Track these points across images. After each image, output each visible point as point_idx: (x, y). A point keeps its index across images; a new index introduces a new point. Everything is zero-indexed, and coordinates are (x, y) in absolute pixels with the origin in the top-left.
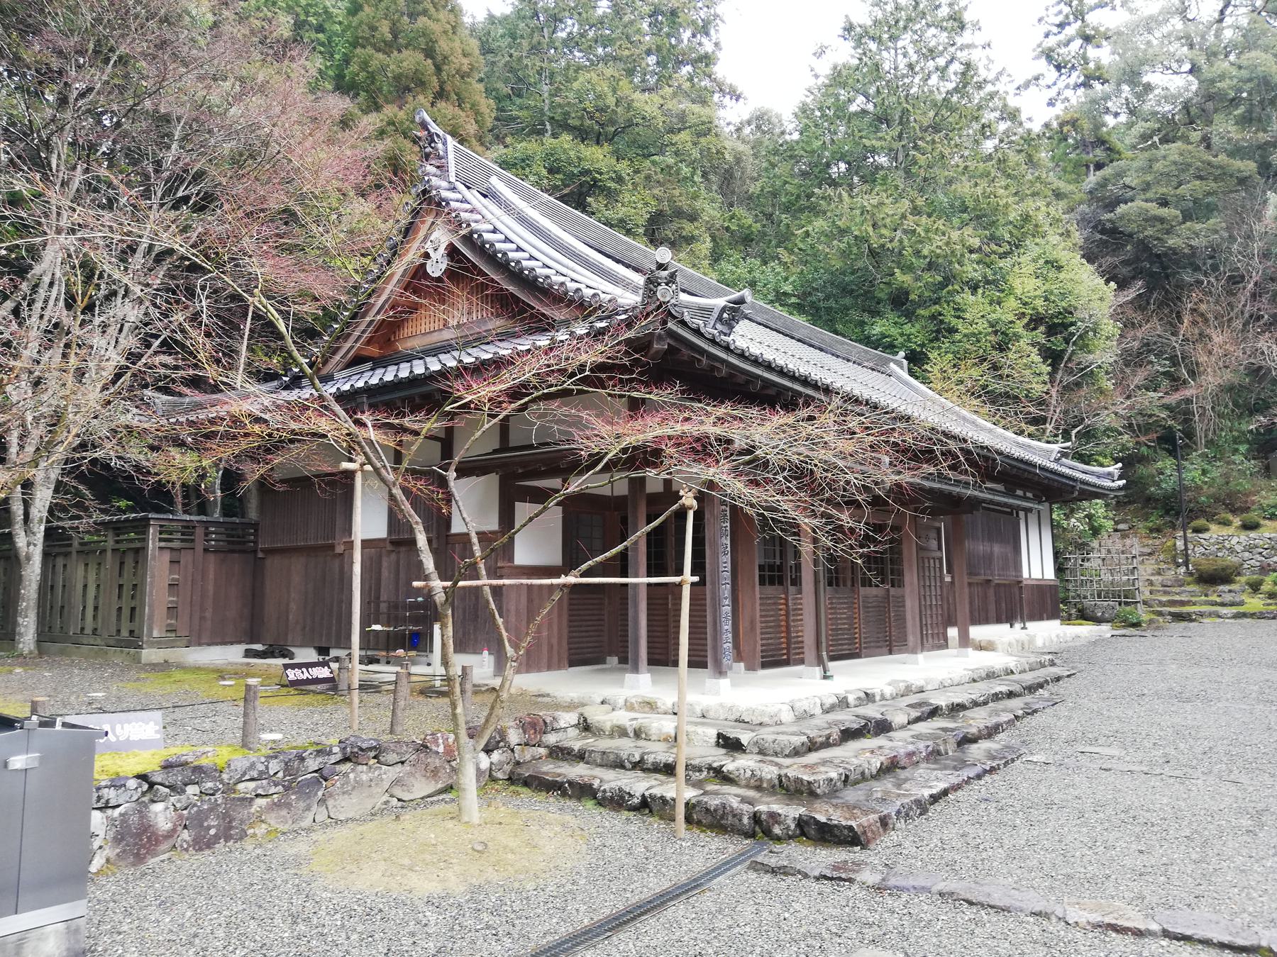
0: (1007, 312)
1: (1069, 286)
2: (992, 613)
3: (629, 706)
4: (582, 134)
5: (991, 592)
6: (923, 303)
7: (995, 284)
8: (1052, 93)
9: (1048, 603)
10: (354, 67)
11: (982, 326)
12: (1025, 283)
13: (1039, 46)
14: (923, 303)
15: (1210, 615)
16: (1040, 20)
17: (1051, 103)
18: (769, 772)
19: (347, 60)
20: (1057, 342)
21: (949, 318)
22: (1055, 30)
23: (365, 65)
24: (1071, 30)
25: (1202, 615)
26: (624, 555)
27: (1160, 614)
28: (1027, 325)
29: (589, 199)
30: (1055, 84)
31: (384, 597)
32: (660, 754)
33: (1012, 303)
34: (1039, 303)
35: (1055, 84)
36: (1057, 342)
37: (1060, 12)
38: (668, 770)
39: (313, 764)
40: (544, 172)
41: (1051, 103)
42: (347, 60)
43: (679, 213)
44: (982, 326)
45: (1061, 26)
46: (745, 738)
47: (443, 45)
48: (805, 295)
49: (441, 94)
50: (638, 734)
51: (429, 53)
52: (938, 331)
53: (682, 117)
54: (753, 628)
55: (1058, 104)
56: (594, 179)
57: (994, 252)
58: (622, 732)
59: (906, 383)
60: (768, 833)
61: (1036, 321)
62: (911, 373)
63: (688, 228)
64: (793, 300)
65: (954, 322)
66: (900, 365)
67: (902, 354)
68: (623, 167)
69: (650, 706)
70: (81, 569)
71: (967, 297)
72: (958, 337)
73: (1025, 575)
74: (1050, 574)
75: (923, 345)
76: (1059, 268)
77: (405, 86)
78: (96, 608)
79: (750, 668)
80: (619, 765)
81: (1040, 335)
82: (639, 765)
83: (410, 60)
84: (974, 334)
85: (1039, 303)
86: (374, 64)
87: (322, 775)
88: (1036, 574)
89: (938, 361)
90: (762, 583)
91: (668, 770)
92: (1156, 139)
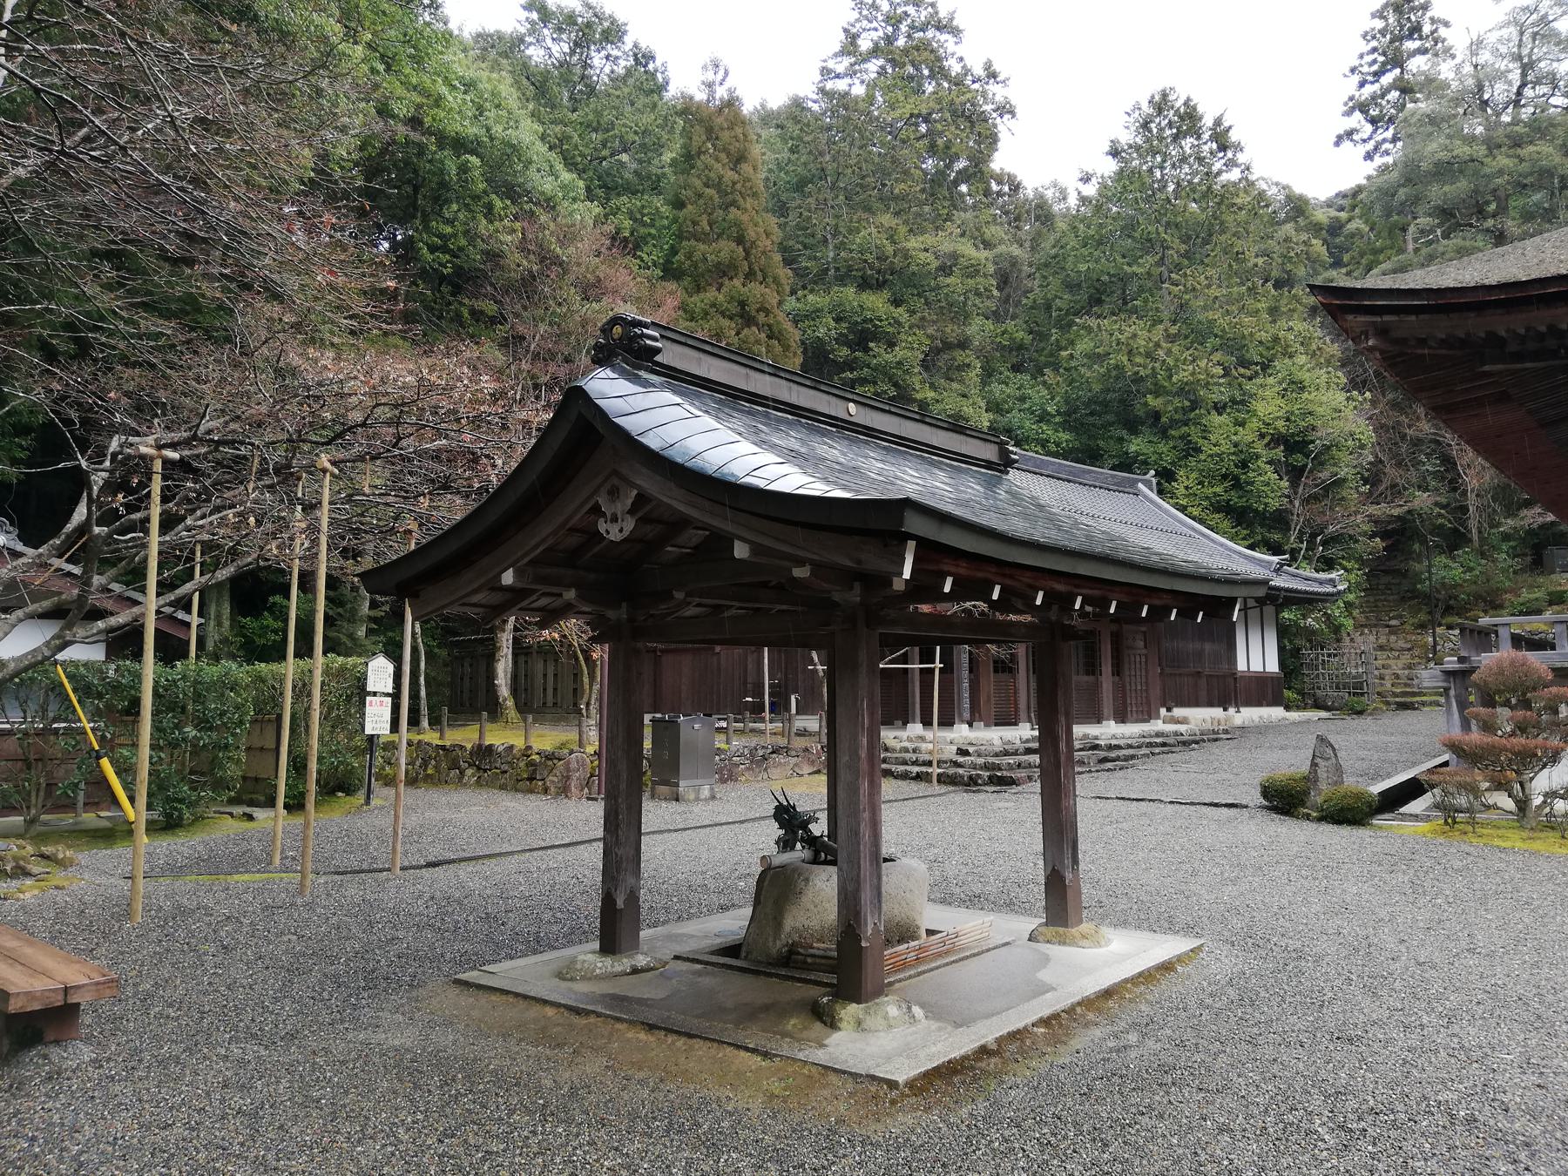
0: (1246, 435)
1: (1311, 407)
2: (1203, 694)
3: (909, 739)
4: (865, 285)
5: (1203, 682)
6: (1174, 423)
7: (1239, 404)
8: (1370, 146)
9: (1261, 691)
10: (680, 257)
11: (1226, 447)
12: (1269, 405)
13: (1351, 99)
14: (1174, 423)
15: (1431, 704)
16: (1353, 70)
17: (1369, 156)
18: (981, 761)
19: (674, 251)
20: (1298, 460)
21: (1195, 437)
22: (1370, 78)
23: (689, 256)
24: (1387, 79)
25: (1423, 704)
26: (905, 654)
27: (1388, 703)
28: (1267, 445)
29: (872, 345)
30: (1370, 138)
31: (750, 680)
32: (927, 757)
33: (1254, 424)
34: (1280, 424)
35: (1370, 138)
36: (1298, 460)
37: (1375, 61)
38: (930, 764)
39: (761, 753)
40: (833, 324)
41: (1369, 156)
42: (674, 251)
43: (948, 346)
44: (1226, 447)
45: (1377, 75)
46: (971, 750)
47: (751, 233)
48: (1068, 414)
49: (750, 275)
50: (914, 751)
51: (740, 240)
52: (1187, 451)
53: (955, 256)
54: (989, 700)
55: (1377, 157)
56: (875, 326)
57: (1242, 376)
58: (906, 750)
59: (1152, 501)
60: (976, 784)
61: (1277, 440)
62: (1160, 492)
63: (961, 356)
64: (1057, 419)
65: (1201, 441)
66: (1148, 484)
67: (1152, 472)
68: (901, 313)
69: (922, 739)
70: (540, 665)
71: (1217, 419)
72: (1203, 457)
73: (1241, 666)
74: (1273, 666)
75: (1173, 463)
76: (1303, 389)
77: (724, 271)
78: (555, 689)
79: (987, 725)
80: (905, 763)
81: (1279, 453)
82: (915, 763)
83: (726, 249)
84: (1218, 455)
85: (1280, 424)
86: (697, 256)
87: (764, 758)
88: (1256, 666)
89: (1185, 480)
90: (996, 671)
91: (930, 764)
92: (1439, 232)
